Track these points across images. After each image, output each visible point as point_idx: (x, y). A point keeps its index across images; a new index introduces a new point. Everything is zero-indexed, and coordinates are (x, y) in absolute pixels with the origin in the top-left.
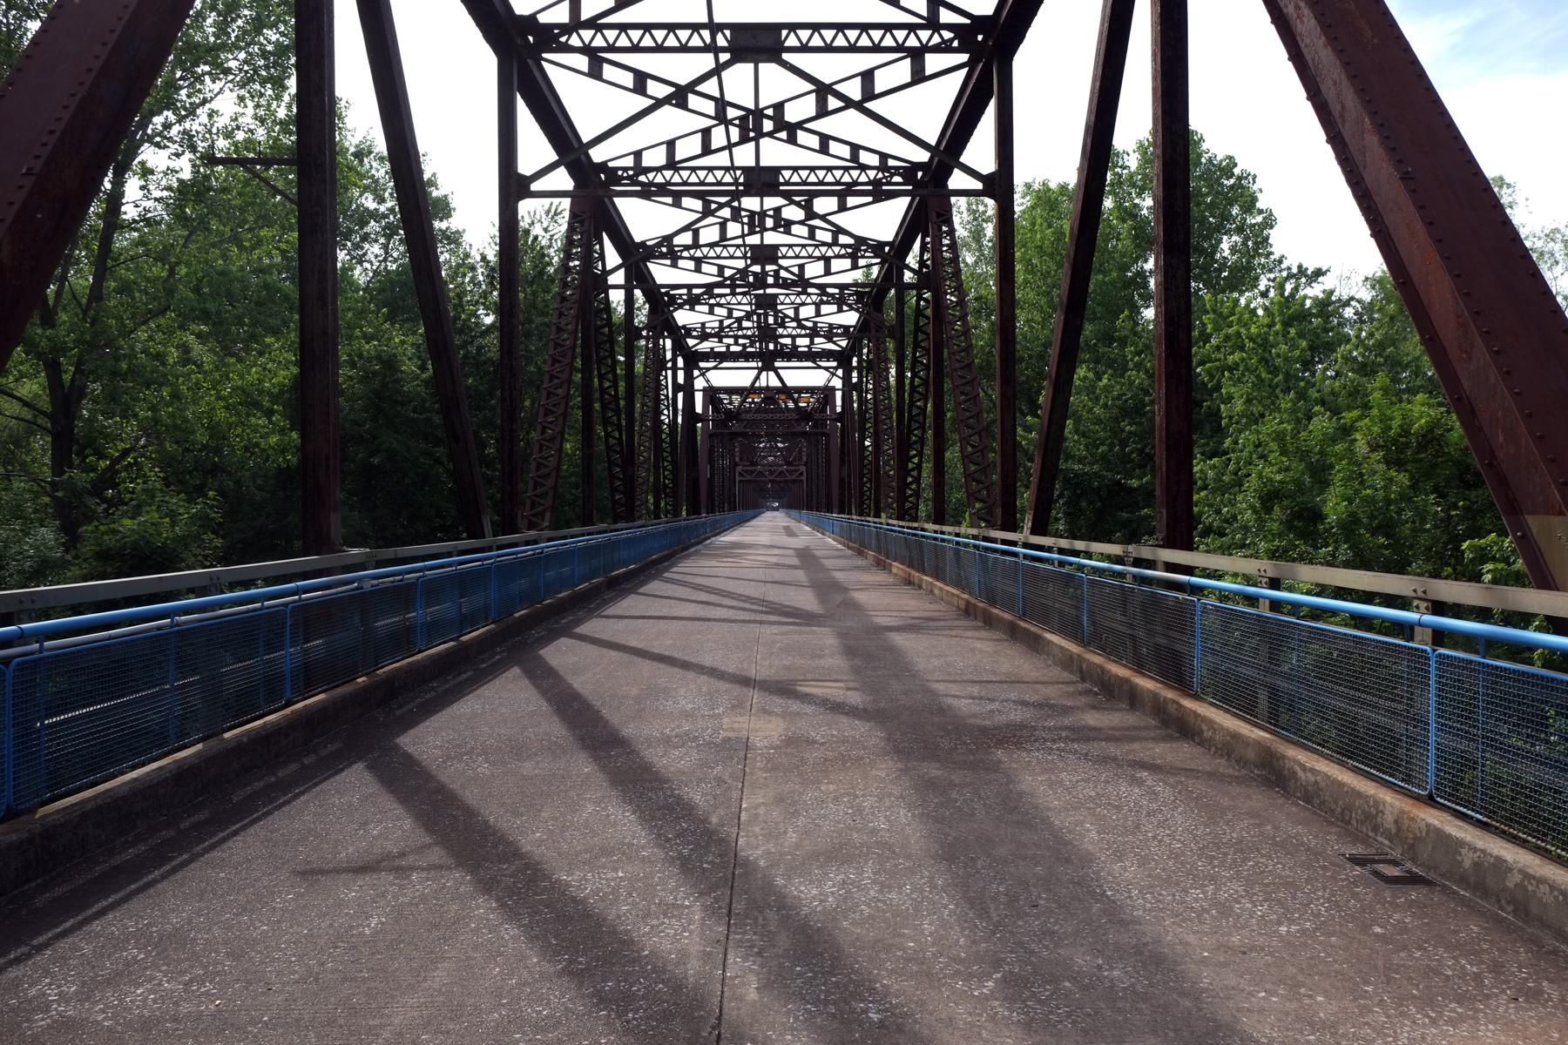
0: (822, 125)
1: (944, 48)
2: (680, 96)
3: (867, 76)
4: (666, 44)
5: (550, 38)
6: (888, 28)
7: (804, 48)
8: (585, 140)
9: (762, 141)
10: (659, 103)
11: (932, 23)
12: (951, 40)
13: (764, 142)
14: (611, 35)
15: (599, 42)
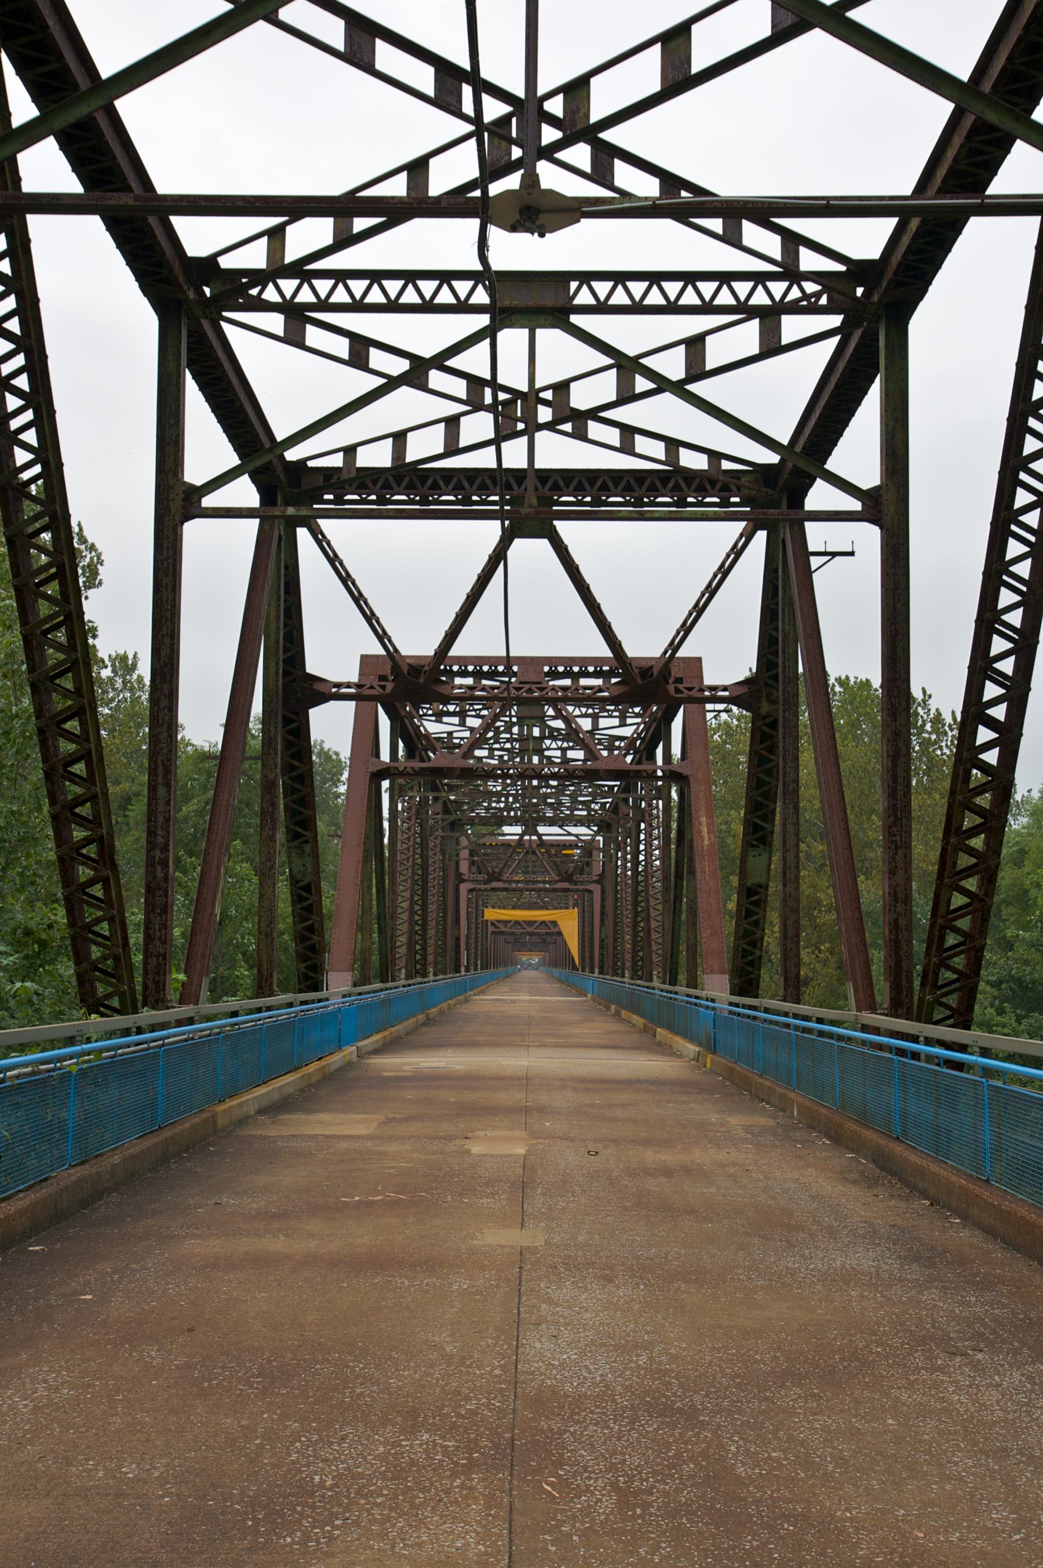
0: (622, 414)
1: (807, 307)
2: (418, 372)
3: (695, 344)
4: (368, 300)
5: (238, 289)
6: (725, 278)
7: (602, 308)
8: (280, 437)
9: (539, 436)
10: (392, 383)
11: (791, 273)
12: (818, 295)
13: (541, 437)
14: (323, 286)
15: (305, 296)
